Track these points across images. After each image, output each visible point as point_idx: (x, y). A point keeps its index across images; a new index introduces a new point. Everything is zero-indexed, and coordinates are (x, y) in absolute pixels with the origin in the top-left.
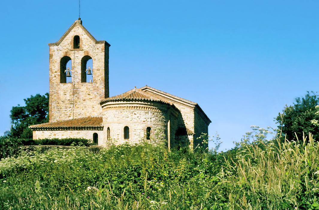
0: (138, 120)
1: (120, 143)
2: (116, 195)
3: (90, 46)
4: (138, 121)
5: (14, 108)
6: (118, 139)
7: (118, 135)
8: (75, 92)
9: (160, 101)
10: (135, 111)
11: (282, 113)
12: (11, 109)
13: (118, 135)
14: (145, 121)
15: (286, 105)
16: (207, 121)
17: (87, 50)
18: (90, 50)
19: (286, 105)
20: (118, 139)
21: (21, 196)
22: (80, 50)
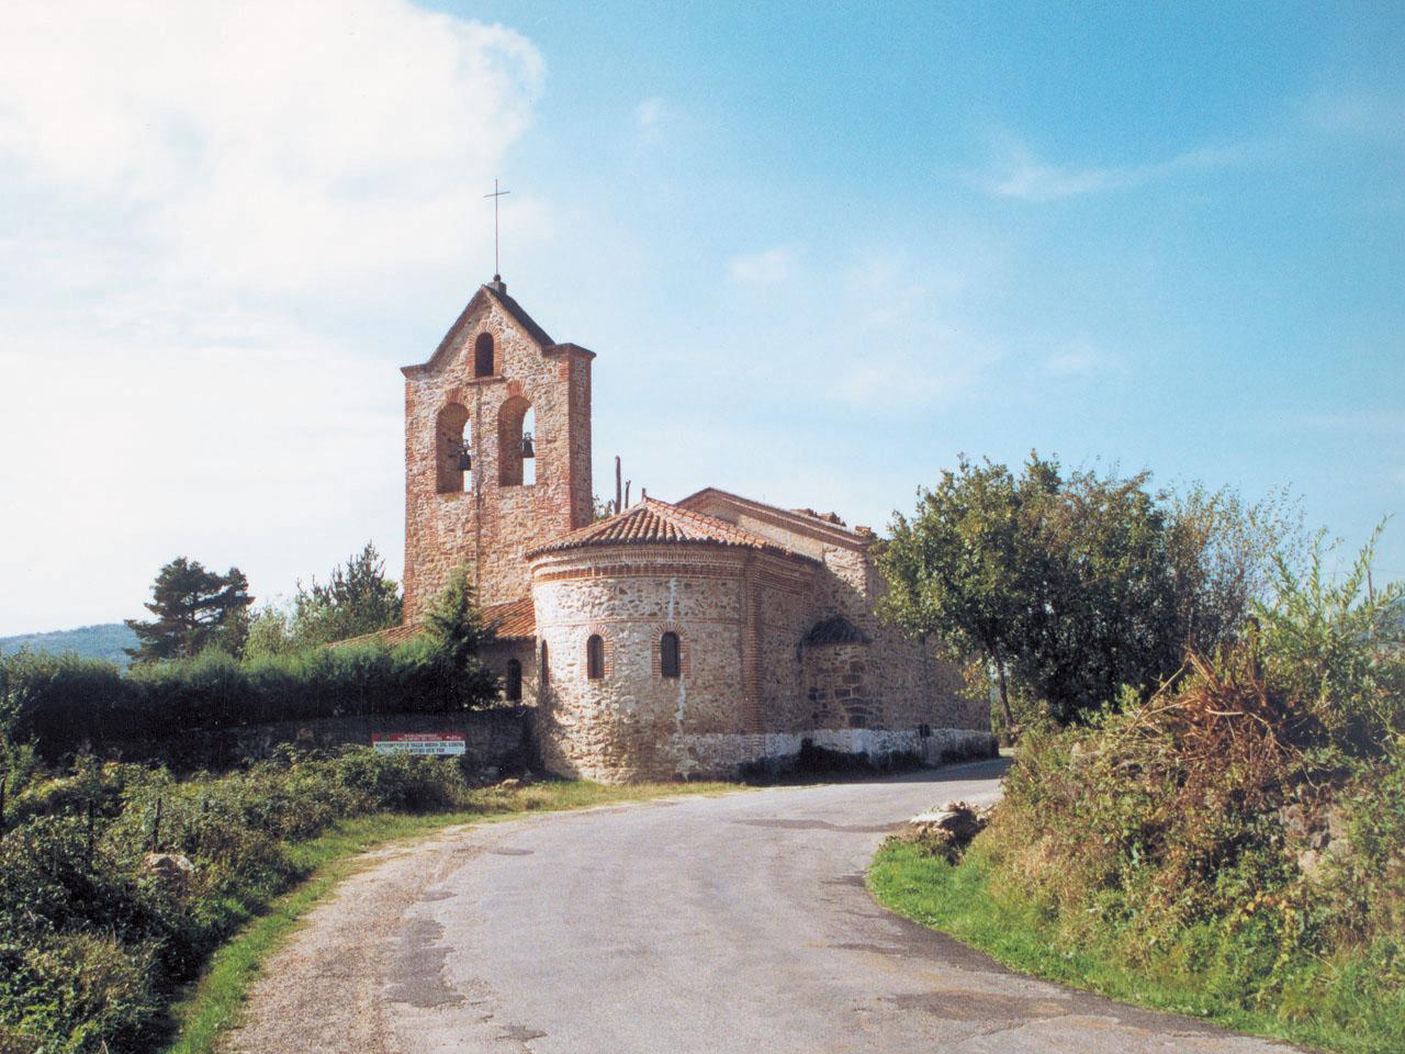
0: (632, 611)
1: (576, 692)
2: (1035, 725)
3: (525, 364)
4: (630, 615)
5: (180, 563)
6: (570, 680)
7: (571, 665)
8: (482, 515)
9: (709, 538)
10: (623, 582)
11: (345, 570)
12: (170, 560)
13: (571, 665)
14: (655, 614)
15: (1034, 456)
16: (819, 626)
17: (517, 378)
18: (526, 377)
19: (1034, 456)
20: (570, 680)
21: (1223, 639)
22: (496, 381)
